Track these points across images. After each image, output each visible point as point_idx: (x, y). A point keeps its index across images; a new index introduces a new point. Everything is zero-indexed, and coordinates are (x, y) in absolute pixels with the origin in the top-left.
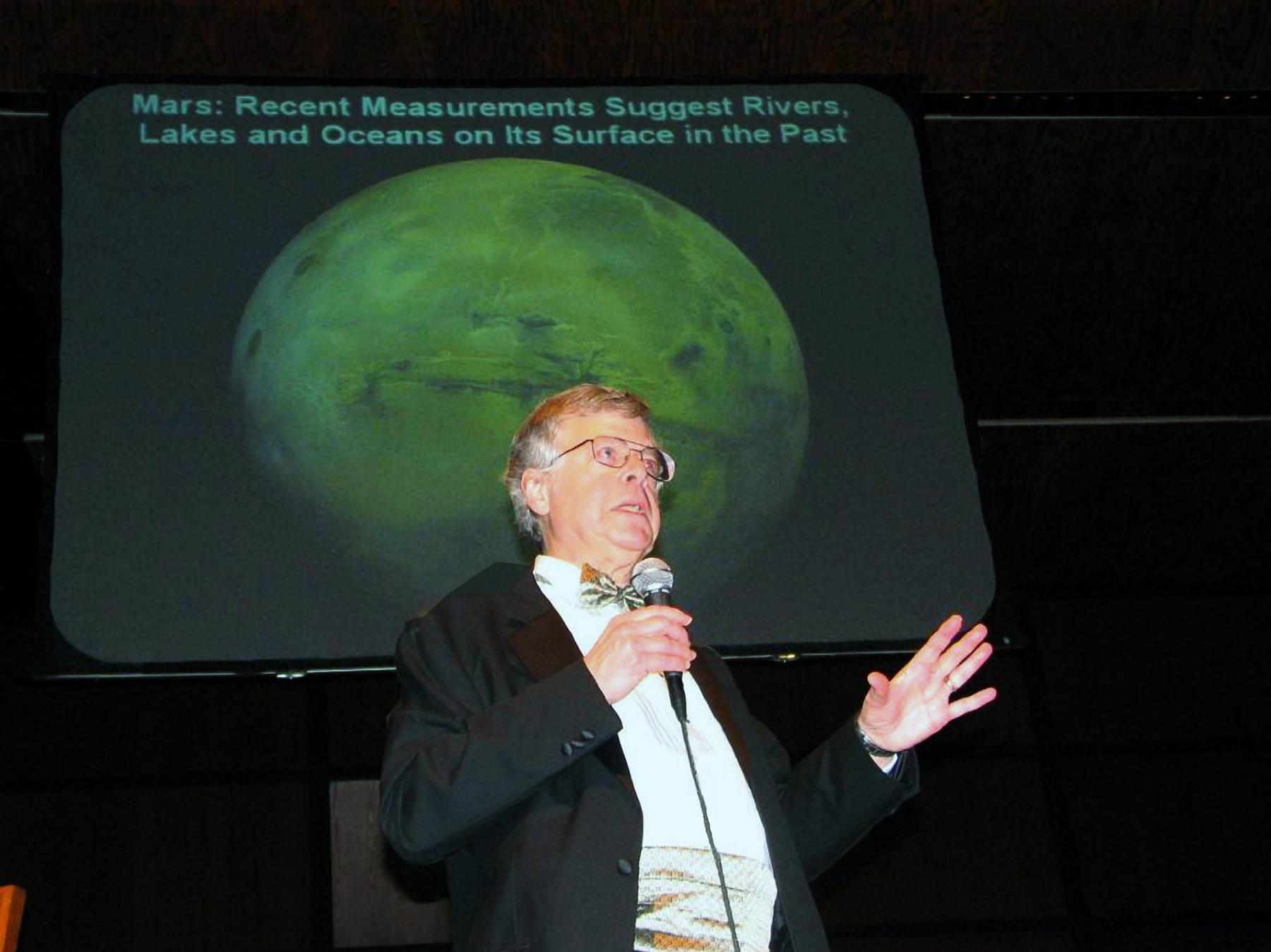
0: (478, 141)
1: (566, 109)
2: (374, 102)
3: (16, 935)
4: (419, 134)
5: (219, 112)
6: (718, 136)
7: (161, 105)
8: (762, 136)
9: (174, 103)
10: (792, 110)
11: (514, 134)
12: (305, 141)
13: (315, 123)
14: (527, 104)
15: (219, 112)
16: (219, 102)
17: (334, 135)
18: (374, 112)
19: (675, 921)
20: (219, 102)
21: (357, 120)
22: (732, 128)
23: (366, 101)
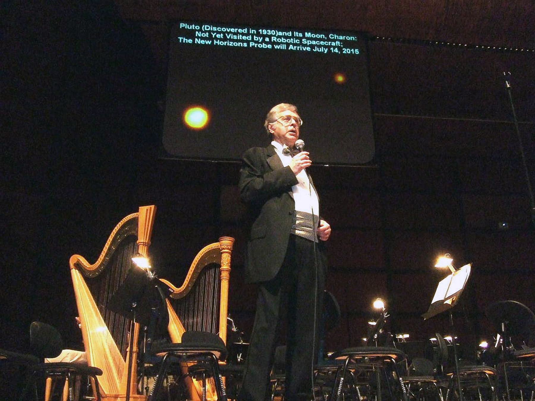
23: (306, 33)
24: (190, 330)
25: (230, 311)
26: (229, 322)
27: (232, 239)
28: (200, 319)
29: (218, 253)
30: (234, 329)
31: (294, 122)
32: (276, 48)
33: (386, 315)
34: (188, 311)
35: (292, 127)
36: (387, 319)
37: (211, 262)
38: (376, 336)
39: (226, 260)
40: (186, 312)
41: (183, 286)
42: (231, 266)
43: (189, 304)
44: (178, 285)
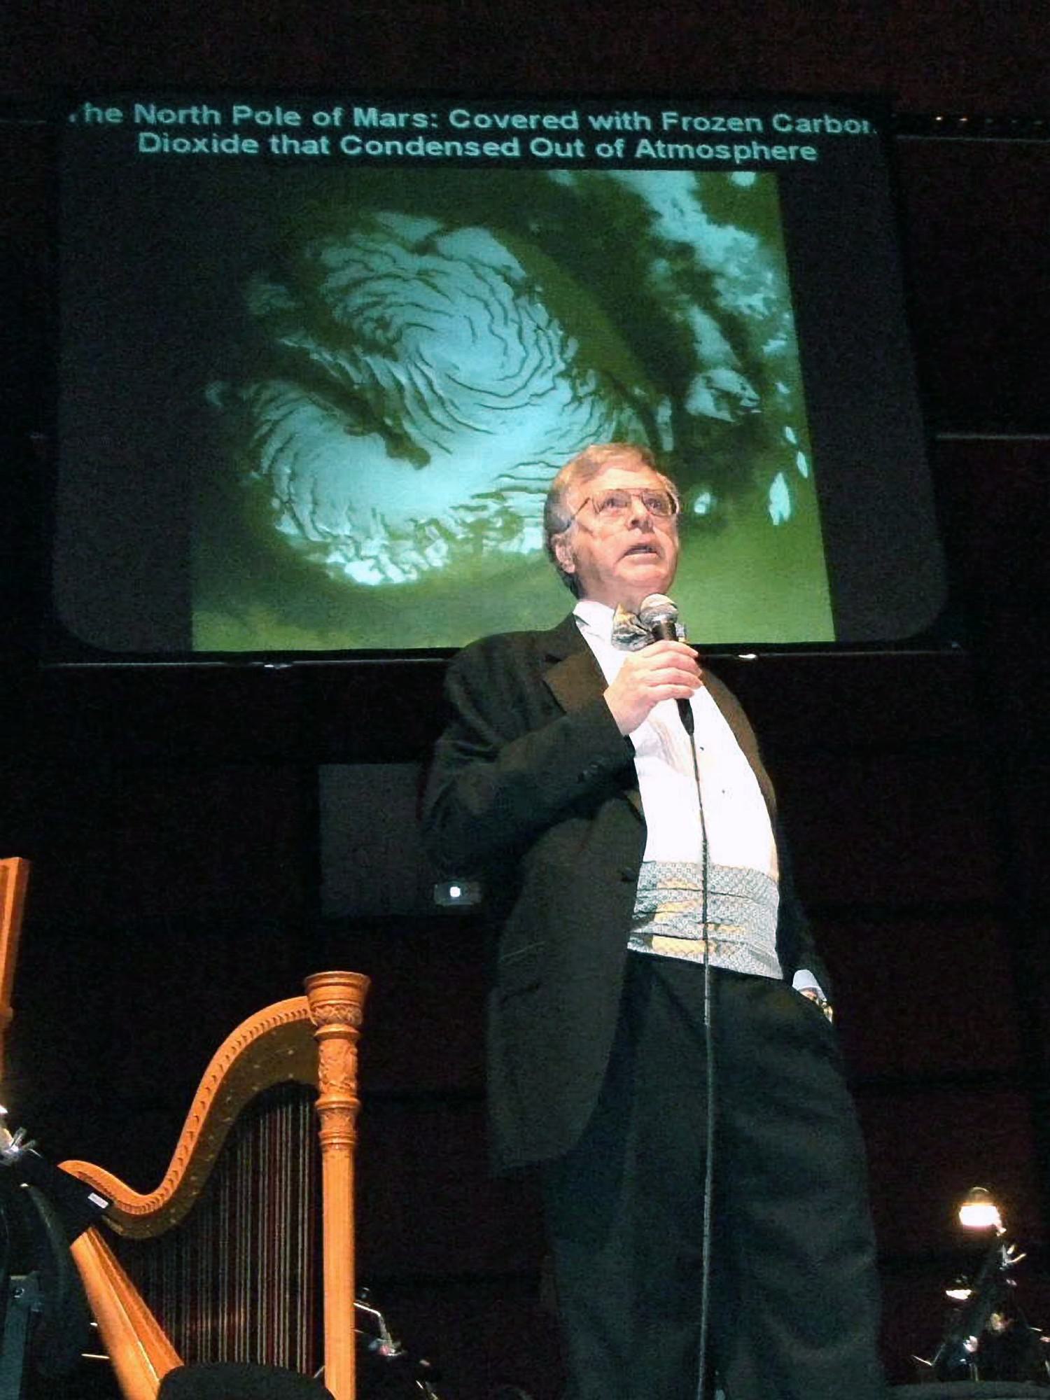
0: (389, 152)
1: (623, 123)
2: (365, 112)
3: (22, 902)
4: (458, 144)
5: (434, 125)
6: (265, 146)
7: (380, 118)
8: (250, 146)
9: (392, 116)
10: (510, 124)
11: (644, 148)
12: (516, 153)
13: (526, 136)
14: (104, 109)
15: (434, 125)
16: (434, 116)
17: (542, 147)
18: (366, 123)
19: (680, 926)
20: (434, 116)
21: (444, 133)
22: (280, 139)
23: (358, 112)
24: (204, 1354)
25: (366, 1280)
26: (362, 1320)
27: (358, 978)
28: (241, 1319)
29: (304, 1037)
30: (389, 1349)
31: (639, 510)
32: (596, 125)
33: (1013, 1256)
34: (194, 1293)
35: (637, 531)
36: (1013, 1271)
37: (277, 1077)
38: (970, 1345)
39: (337, 1069)
40: (185, 1294)
41: (165, 1183)
42: (361, 1093)
43: (195, 1252)
44: (145, 1184)
